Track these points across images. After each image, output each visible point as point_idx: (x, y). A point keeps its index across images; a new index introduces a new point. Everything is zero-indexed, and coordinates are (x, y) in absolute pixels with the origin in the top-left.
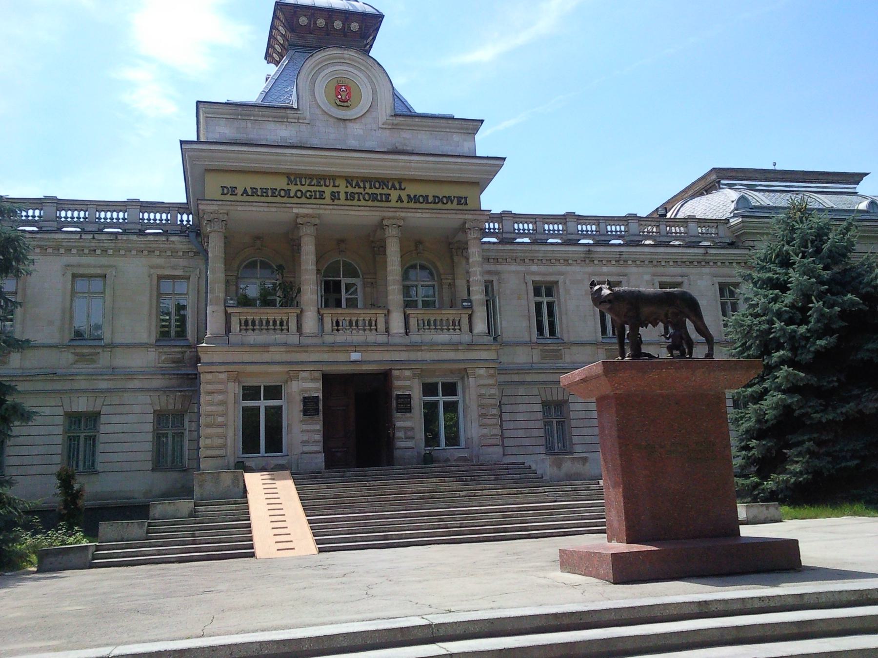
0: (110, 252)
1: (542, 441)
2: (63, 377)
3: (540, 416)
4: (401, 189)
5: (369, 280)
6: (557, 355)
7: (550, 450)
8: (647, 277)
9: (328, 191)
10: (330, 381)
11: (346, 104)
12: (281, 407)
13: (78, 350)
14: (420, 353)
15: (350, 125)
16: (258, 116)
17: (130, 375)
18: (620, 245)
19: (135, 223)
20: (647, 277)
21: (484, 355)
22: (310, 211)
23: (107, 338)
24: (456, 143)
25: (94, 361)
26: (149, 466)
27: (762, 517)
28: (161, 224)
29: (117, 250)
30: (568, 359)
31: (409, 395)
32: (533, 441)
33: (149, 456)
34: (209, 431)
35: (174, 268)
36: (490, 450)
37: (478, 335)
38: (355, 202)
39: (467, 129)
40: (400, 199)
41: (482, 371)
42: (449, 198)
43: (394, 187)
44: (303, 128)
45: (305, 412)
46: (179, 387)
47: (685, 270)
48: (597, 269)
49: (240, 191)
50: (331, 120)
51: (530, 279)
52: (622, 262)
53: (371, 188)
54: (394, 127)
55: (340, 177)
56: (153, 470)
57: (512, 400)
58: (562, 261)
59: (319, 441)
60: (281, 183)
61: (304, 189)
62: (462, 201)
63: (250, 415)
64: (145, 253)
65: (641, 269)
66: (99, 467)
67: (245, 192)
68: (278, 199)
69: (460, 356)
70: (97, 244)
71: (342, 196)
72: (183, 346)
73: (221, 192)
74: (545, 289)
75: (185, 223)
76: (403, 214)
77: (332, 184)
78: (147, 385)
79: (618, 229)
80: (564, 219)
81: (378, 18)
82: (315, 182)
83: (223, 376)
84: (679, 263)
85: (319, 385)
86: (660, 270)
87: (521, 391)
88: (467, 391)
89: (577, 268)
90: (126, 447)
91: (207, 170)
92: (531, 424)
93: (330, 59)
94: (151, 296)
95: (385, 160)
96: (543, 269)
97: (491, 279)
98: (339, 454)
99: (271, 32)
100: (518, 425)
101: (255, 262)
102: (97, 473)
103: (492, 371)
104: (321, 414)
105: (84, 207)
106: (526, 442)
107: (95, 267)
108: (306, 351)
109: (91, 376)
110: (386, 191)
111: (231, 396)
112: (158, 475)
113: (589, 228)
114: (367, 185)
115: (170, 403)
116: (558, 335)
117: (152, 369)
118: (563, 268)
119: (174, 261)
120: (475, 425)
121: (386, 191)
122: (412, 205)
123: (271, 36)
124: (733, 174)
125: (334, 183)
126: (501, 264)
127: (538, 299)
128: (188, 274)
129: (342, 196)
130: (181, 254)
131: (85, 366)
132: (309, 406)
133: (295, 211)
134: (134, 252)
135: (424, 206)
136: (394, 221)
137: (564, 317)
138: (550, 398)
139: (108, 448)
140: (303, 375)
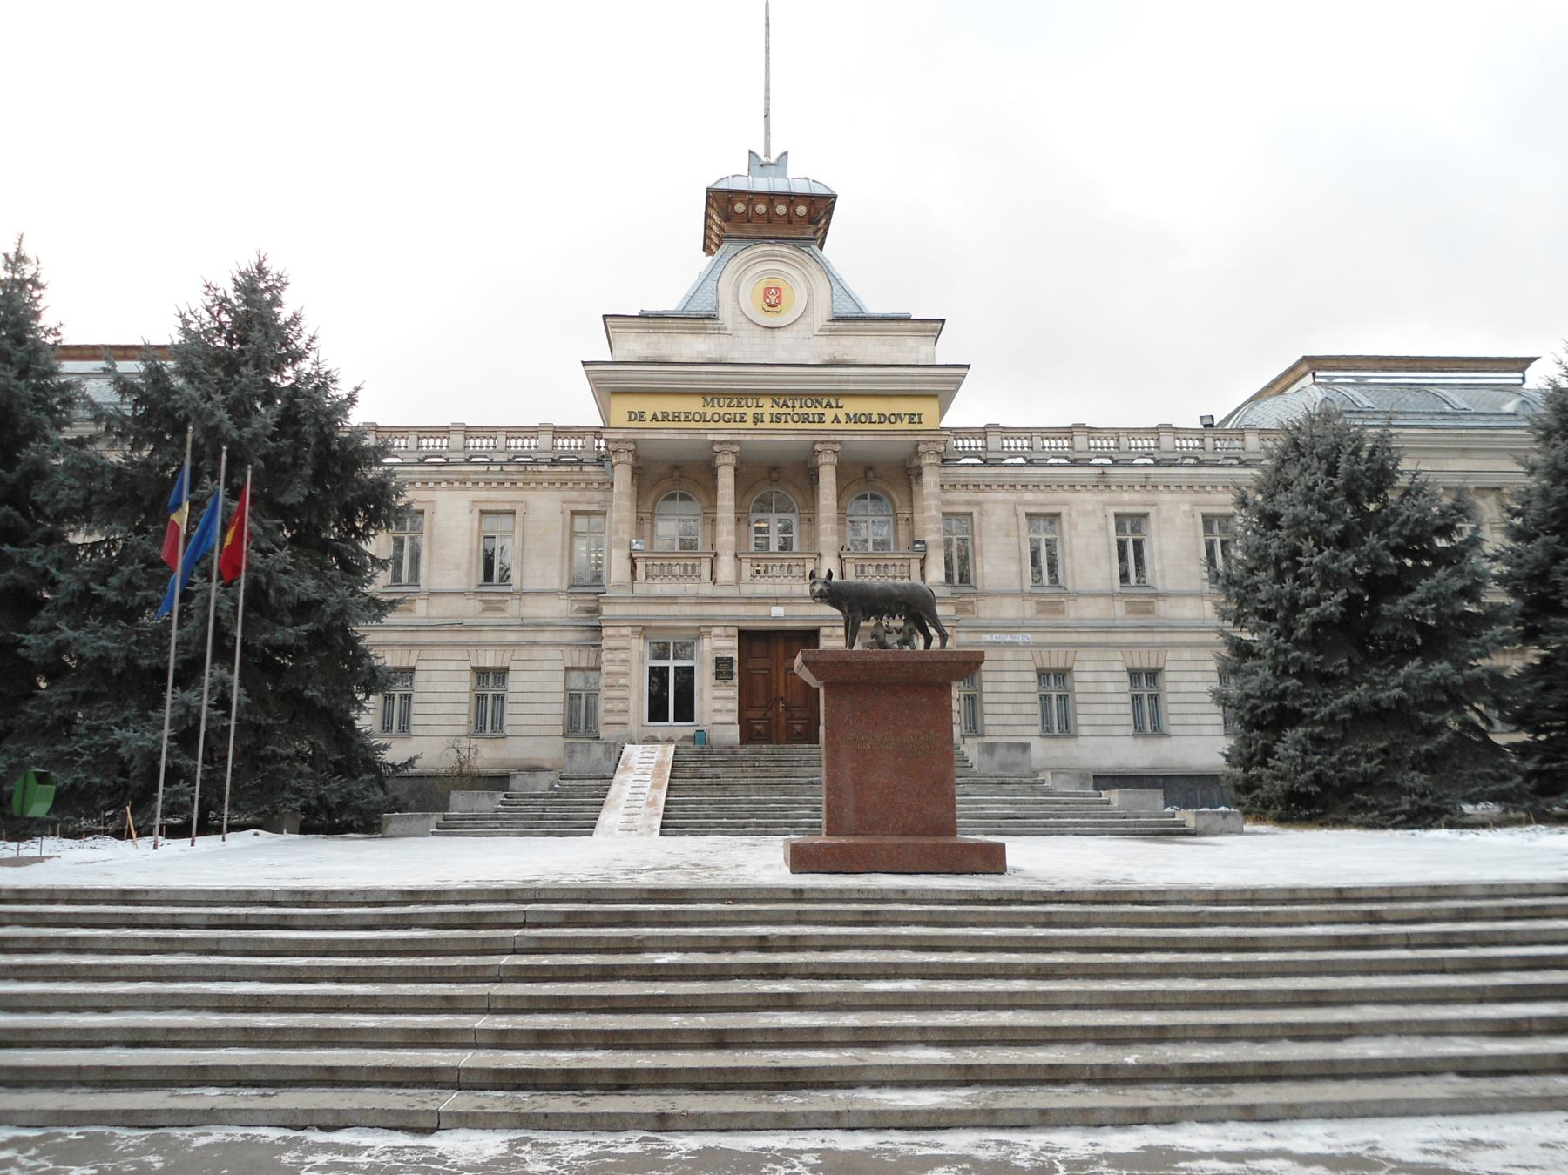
0: (520, 485)
2: (471, 628)
3: (1034, 687)
6: (1057, 608)
7: (1047, 731)
8: (1185, 507)
9: (750, 412)
10: (747, 637)
15: (778, 333)
18: (1146, 465)
27: (1217, 828)
30: (1072, 613)
32: (1024, 720)
33: (559, 720)
34: (611, 694)
38: (782, 425)
40: (836, 419)
43: (829, 404)
45: (718, 675)
48: (1116, 497)
49: (648, 416)
54: (832, 333)
56: (564, 736)
61: (722, 411)
63: (658, 675)
65: (1176, 497)
66: (507, 731)
67: (655, 417)
71: (767, 418)
76: (839, 438)
78: (558, 638)
80: (1069, 432)
81: (835, 197)
83: (627, 631)
85: (734, 643)
86: (1204, 497)
89: (1087, 496)
90: (537, 708)
92: (1021, 698)
96: (1040, 497)
98: (759, 727)
100: (1004, 698)
102: (504, 737)
106: (1014, 720)
109: (499, 627)
113: (1105, 443)
114: (797, 404)
122: (851, 426)
123: (707, 227)
124: (1334, 364)
129: (767, 418)
132: (722, 669)
133: (711, 437)
135: (867, 426)
136: (829, 446)
137: (1068, 560)
138: (1047, 665)
140: (716, 631)
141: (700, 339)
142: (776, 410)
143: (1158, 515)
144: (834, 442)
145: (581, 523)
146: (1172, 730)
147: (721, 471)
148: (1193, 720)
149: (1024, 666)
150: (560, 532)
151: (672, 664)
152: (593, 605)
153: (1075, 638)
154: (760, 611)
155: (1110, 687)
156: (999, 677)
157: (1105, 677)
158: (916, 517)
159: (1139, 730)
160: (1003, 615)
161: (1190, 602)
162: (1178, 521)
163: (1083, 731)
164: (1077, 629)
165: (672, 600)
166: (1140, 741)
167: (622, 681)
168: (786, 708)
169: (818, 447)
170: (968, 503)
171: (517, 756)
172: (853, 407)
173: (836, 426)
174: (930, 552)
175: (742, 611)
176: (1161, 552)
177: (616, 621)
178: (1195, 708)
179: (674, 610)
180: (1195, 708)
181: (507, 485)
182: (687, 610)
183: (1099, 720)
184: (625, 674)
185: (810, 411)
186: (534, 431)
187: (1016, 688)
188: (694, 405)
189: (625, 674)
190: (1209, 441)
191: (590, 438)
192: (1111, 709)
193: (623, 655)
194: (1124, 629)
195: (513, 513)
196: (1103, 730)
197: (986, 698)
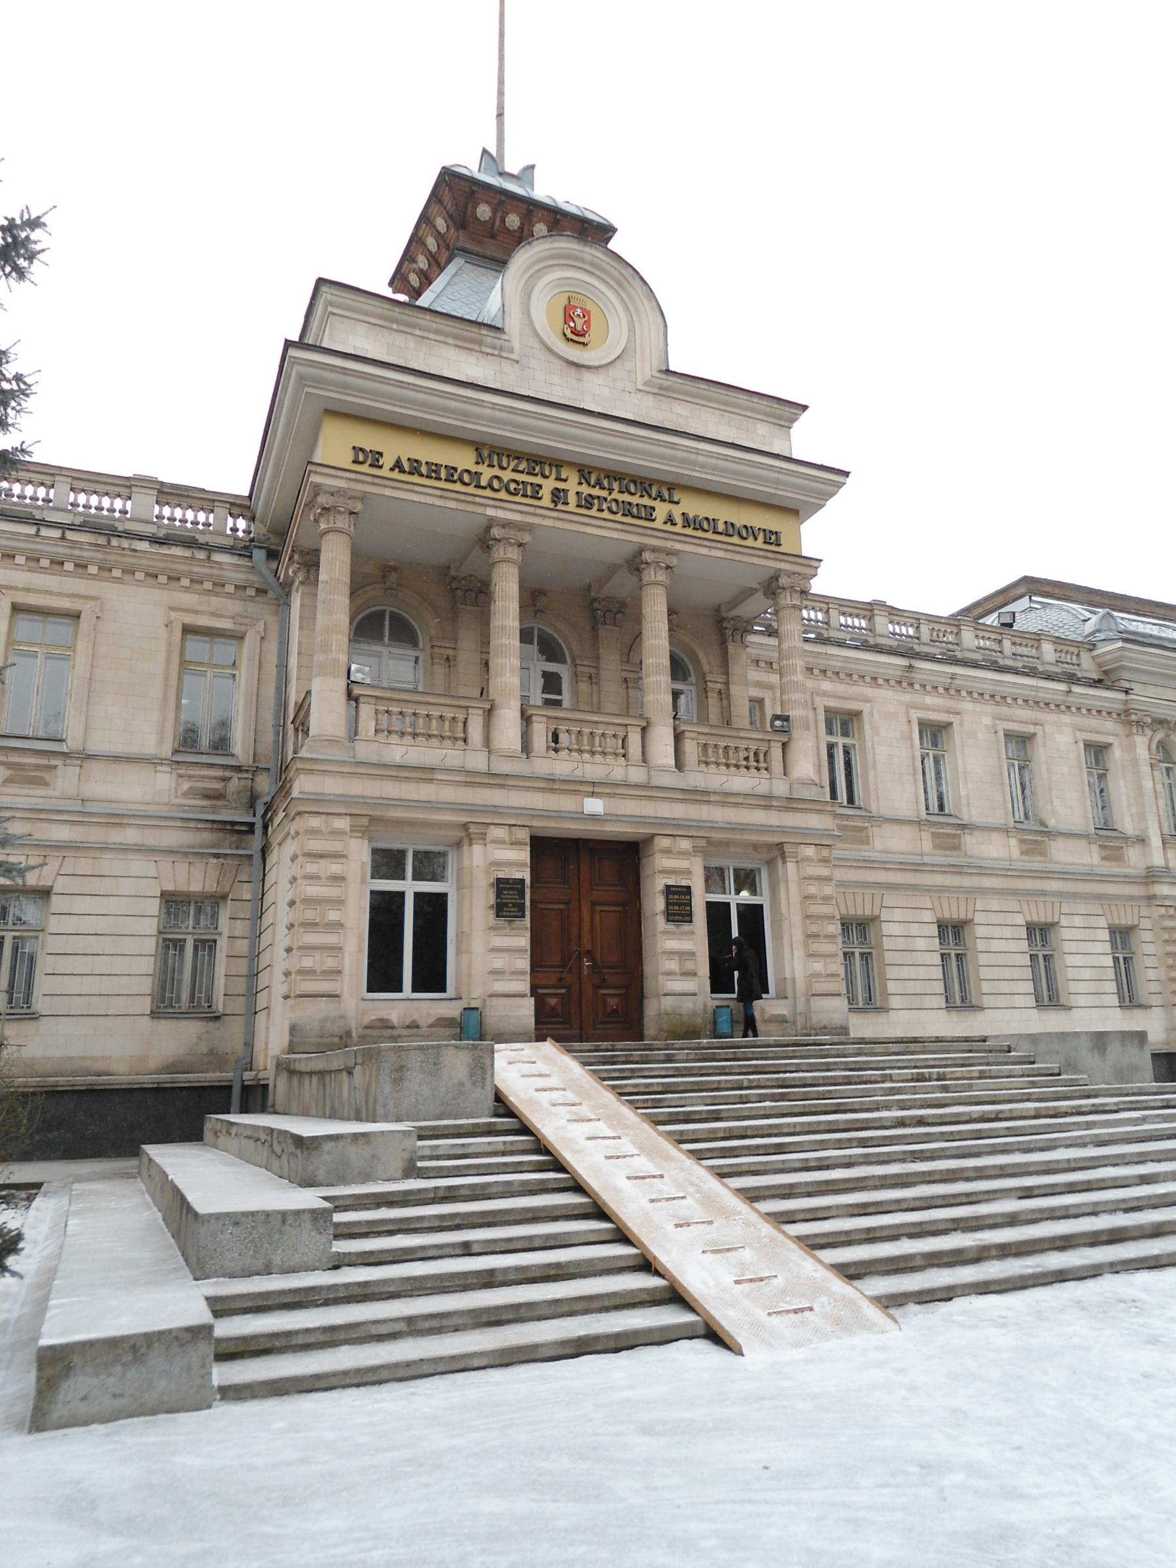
0: (93, 569)
5: (586, 669)
6: (861, 836)
9: (548, 485)
10: (545, 848)
11: (581, 339)
13: (14, 758)
14: (705, 808)
15: (588, 376)
16: (429, 330)
20: (987, 721)
22: (517, 517)
23: (73, 741)
24: (760, 435)
25: (44, 783)
26: (146, 1005)
29: (105, 568)
30: (878, 844)
31: (689, 888)
33: (146, 986)
36: (828, 1003)
37: (804, 783)
39: (780, 418)
40: (670, 520)
44: (507, 366)
45: (500, 909)
46: (213, 846)
47: (1039, 715)
48: (917, 698)
49: (388, 461)
50: (556, 361)
52: (952, 692)
55: (571, 464)
58: (868, 679)
59: (523, 973)
60: (464, 459)
61: (507, 475)
62: (773, 538)
63: (385, 911)
64: (163, 579)
65: (978, 707)
66: (40, 1004)
67: (398, 465)
68: (458, 487)
69: (774, 819)
70: (68, 551)
71: (572, 499)
72: (225, 767)
73: (350, 456)
75: (240, 534)
76: (678, 546)
77: (553, 476)
81: (614, 230)
83: (342, 824)
84: (1031, 703)
85: (524, 855)
86: (1004, 710)
88: (782, 886)
90: (101, 965)
91: (329, 412)
93: (559, 257)
94: (168, 662)
99: (417, 227)
102: (34, 1017)
104: (528, 913)
105: (48, 480)
107: (60, 594)
108: (503, 786)
109: (38, 814)
110: (646, 501)
112: (164, 1026)
114: (616, 485)
115: (195, 879)
116: (857, 803)
118: (869, 691)
119: (216, 602)
120: (799, 953)
121: (646, 501)
125: (558, 473)
128: (243, 628)
129: (572, 499)
131: (25, 791)
132: (506, 899)
133: (491, 512)
134: (140, 576)
136: (662, 557)
137: (871, 773)
139: (62, 965)
141: (472, 358)
142: (586, 490)
143: (961, 724)
145: (197, 648)
146: (987, 1001)
148: (1005, 987)
150: (161, 657)
151: (410, 887)
152: (217, 785)
154: (566, 803)
155: (921, 944)
157: (915, 929)
159: (950, 1006)
161: (996, 837)
162: (980, 736)
163: (895, 1002)
164: (885, 866)
165: (425, 773)
167: (333, 916)
168: (593, 968)
171: (59, 1053)
174: (796, 733)
176: (965, 773)
177: (320, 805)
178: (1006, 973)
179: (426, 792)
180: (1006, 973)
181: (69, 566)
182: (448, 794)
183: (911, 987)
184: (339, 903)
185: (635, 500)
186: (126, 486)
188: (464, 459)
189: (339, 903)
190: (1007, 644)
191: (63, 486)
193: (335, 868)
194: (934, 869)
195: (77, 616)
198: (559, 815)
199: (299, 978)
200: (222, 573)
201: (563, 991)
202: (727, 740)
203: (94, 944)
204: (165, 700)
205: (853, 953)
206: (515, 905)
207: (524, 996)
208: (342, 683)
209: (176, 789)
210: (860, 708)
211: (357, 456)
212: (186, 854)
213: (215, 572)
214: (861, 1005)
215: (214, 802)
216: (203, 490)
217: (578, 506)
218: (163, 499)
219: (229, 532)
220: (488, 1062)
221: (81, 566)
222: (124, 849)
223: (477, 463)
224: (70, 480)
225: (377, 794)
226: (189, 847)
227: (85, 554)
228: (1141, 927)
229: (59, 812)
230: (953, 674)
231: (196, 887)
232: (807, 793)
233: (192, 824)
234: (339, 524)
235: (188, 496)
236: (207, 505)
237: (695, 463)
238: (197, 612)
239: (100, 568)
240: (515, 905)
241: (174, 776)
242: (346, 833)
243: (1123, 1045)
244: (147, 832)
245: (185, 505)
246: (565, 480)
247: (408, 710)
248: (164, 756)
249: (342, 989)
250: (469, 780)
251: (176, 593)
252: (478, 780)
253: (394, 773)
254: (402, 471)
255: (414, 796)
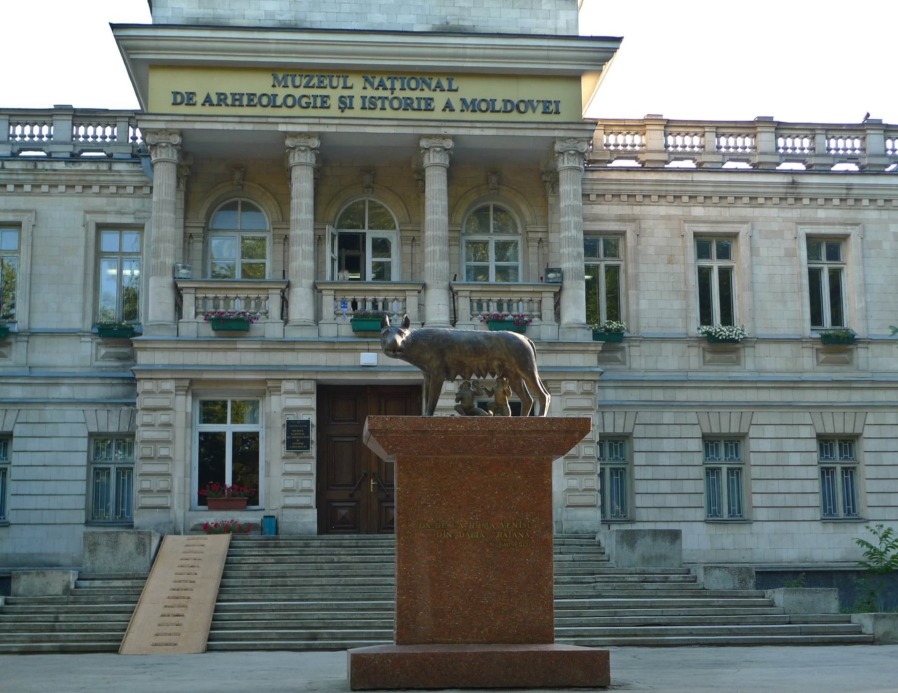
1: (702, 500)
3: (699, 459)
4: (450, 90)
9: (334, 96)
10: (329, 395)
12: (234, 434)
17: (54, 379)
19: (65, 143)
21: (577, 360)
26: (81, 517)
28: (104, 144)
32: (684, 501)
35: (120, 213)
36: (580, 513)
37: (570, 328)
38: (377, 113)
40: (448, 107)
41: (572, 386)
42: (529, 103)
45: (290, 444)
46: (125, 397)
48: (808, 213)
49: (200, 99)
51: (690, 229)
52: (851, 202)
53: (403, 89)
56: (87, 523)
57: (651, 431)
61: (297, 93)
63: (211, 446)
65: (885, 215)
67: (208, 101)
70: (8, 177)
71: (357, 103)
73: (171, 99)
74: (713, 245)
76: (452, 131)
77: (341, 85)
78: (80, 393)
79: (849, 145)
82: (315, 81)
83: (169, 386)
85: (311, 402)
87: (668, 417)
89: (773, 212)
90: (49, 487)
92: (682, 473)
95: (426, 45)
96: (713, 212)
97: (623, 228)
98: (343, 512)
100: (660, 473)
101: (236, 203)
102: (749, 522)
103: (587, 387)
106: (672, 501)
108: (293, 350)
110: (427, 94)
111: (179, 420)
114: (398, 85)
117: (88, 370)
118: (748, 212)
121: (427, 94)
122: (468, 116)
125: (345, 82)
126: (640, 204)
127: (705, 263)
129: (357, 103)
130: (130, 190)
132: (296, 436)
133: (282, 128)
135: (488, 116)
138: (715, 430)
139: (24, 488)
140: (287, 386)
142: (370, 92)
144: (444, 137)
145: (110, 241)
146: (760, 514)
147: (296, 173)
149: (687, 431)
151: (229, 429)
153: (751, 396)
155: (795, 459)
156: (655, 445)
157: (789, 445)
158: (552, 237)
159: (829, 514)
160: (661, 365)
162: (886, 245)
164: (756, 385)
166: (830, 528)
167: (163, 452)
169: (424, 143)
170: (621, 219)
171: (24, 551)
172: (471, 90)
173: (448, 115)
174: (567, 283)
175: (322, 359)
177: (153, 372)
183: (779, 500)
184: (167, 442)
185: (414, 95)
187: (676, 459)
188: (261, 84)
189: (167, 442)
192: (795, 486)
193: (163, 418)
196: (784, 514)
197: (638, 473)
198: (339, 370)
199: (140, 495)
200: (122, 178)
201: (353, 504)
202: (500, 295)
203: (43, 473)
204: (85, 284)
205: (834, 468)
206: (301, 440)
207: (311, 507)
208: (170, 279)
209: (97, 354)
210: (736, 230)
211: (175, 99)
212: (105, 404)
213: (117, 178)
214: (726, 517)
215: (124, 363)
216: (107, 110)
217: (363, 108)
218: (78, 121)
219: (130, 141)
220: (147, 541)
221: (19, 186)
222: (61, 403)
223: (274, 86)
224: (7, 117)
225: (194, 362)
226: (107, 398)
227: (21, 177)
228: (865, 435)
229: (14, 377)
230: (847, 184)
231: (113, 429)
232: (571, 337)
233: (108, 381)
234: (164, 157)
235: (96, 117)
236: (111, 121)
237: (465, 56)
238: (106, 212)
239: (33, 186)
240: (301, 440)
241: (94, 345)
242: (172, 393)
243: (654, 541)
244: (77, 388)
245: (94, 124)
246: (351, 88)
247: (221, 295)
248: (86, 330)
249: (172, 503)
250: (264, 347)
251: (90, 199)
252: (271, 347)
253: (205, 346)
254: (212, 105)
255: (223, 362)
